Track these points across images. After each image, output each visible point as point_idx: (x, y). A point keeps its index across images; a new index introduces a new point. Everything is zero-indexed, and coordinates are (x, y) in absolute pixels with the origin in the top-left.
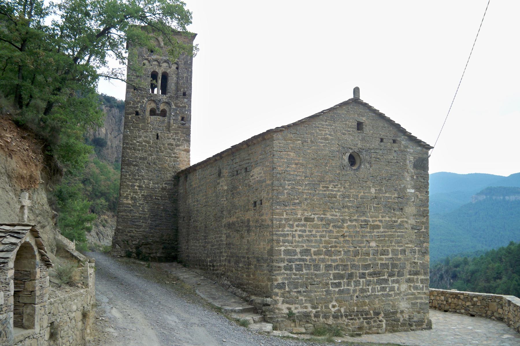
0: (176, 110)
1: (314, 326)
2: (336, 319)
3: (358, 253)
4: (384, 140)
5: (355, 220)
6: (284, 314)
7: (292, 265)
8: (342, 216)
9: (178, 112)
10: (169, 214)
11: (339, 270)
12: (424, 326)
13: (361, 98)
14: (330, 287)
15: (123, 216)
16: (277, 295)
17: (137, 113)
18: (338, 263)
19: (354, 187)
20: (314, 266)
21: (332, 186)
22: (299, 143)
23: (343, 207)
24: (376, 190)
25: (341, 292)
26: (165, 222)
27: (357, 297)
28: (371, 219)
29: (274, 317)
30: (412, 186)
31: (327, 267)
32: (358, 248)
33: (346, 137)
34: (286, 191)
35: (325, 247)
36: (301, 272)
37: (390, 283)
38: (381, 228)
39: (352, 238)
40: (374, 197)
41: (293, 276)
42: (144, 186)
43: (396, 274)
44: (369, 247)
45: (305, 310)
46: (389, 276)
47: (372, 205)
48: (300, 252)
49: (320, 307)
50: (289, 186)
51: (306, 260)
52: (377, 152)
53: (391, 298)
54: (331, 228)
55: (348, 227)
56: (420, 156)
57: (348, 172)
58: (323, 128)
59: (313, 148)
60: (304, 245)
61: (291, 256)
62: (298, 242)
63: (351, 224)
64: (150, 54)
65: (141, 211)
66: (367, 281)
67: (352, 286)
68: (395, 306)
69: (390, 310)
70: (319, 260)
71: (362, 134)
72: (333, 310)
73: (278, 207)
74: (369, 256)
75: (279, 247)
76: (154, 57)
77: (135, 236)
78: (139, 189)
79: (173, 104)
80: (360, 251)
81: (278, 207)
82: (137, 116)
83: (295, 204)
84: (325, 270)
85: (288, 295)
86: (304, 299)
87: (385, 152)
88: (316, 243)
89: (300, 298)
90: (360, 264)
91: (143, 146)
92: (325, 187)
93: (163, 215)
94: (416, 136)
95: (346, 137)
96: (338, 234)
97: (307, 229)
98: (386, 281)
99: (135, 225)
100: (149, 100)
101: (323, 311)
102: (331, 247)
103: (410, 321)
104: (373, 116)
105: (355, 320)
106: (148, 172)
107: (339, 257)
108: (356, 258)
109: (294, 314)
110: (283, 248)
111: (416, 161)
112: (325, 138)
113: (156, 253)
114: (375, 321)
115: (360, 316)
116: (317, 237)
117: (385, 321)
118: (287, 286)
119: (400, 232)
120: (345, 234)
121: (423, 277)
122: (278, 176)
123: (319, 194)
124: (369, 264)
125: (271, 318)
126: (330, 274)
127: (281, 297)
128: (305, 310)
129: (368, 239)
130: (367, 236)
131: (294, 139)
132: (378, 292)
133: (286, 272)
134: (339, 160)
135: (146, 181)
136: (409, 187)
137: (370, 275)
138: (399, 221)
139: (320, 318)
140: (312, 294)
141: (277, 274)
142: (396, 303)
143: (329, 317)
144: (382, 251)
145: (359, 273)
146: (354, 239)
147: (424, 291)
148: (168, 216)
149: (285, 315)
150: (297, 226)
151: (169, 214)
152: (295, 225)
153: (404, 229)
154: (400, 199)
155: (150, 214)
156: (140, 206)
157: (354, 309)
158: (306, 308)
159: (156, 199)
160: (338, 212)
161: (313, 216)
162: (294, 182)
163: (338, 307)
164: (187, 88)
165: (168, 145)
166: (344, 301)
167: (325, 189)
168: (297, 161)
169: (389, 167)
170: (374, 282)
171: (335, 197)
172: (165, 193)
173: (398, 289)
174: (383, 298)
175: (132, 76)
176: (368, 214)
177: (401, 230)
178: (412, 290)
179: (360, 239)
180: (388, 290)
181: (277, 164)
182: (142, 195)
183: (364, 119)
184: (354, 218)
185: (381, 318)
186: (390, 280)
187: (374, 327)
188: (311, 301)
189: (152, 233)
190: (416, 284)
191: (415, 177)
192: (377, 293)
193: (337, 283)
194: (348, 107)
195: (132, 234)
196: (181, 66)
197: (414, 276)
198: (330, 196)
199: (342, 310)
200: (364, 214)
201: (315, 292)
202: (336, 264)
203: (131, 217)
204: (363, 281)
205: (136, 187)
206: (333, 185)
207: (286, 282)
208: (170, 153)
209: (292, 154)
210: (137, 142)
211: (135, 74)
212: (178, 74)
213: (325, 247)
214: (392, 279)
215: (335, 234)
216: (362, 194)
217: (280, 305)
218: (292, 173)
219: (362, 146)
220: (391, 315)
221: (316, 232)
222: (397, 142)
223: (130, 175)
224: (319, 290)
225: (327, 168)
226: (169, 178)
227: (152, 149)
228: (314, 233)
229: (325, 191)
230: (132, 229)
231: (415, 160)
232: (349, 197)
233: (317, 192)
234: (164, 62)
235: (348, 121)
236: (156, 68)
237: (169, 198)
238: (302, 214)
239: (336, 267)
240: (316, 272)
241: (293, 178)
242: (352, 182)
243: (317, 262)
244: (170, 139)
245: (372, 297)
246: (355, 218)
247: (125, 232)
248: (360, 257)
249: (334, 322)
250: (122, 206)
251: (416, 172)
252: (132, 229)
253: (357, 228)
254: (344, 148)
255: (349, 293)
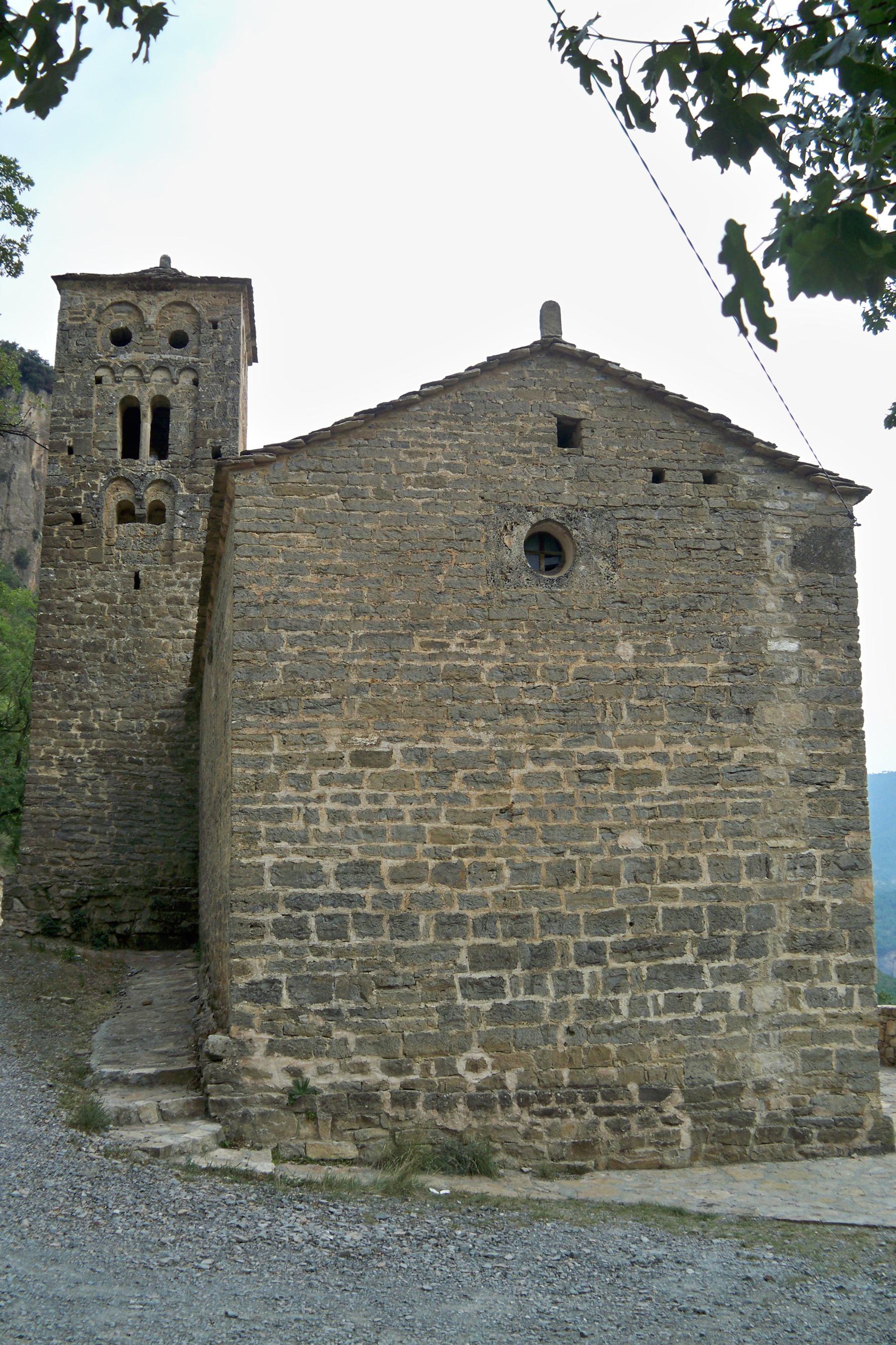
0: (193, 501)
1: (393, 1137)
2: (481, 1113)
3: (569, 874)
4: (668, 475)
5: (556, 755)
6: (277, 1090)
7: (305, 919)
8: (502, 742)
9: (197, 507)
10: (170, 806)
11: (494, 936)
12: (862, 1141)
13: (565, 337)
14: (459, 996)
15: (35, 815)
16: (246, 1021)
17: (78, 519)
18: (491, 908)
19: (547, 641)
20: (392, 919)
21: (460, 641)
22: (330, 502)
23: (506, 713)
24: (638, 648)
25: (501, 1014)
26: (160, 829)
27: (570, 1031)
28: (619, 753)
29: (232, 1101)
30: (790, 631)
31: (443, 924)
32: (568, 855)
33: (515, 471)
34: (280, 665)
35: (436, 854)
36: (339, 944)
37: (709, 982)
38: (665, 782)
39: (545, 819)
40: (634, 673)
41: (310, 958)
42: (97, 726)
43: (733, 948)
44: (616, 850)
45: (359, 1078)
46: (703, 955)
47: (622, 700)
48: (336, 874)
49: (417, 1067)
50: (292, 645)
51: (361, 901)
52: (639, 515)
53: (714, 1036)
54: (457, 786)
55: (526, 780)
56: (819, 521)
57: (524, 591)
58: (421, 445)
59: (387, 513)
60: (354, 847)
61: (302, 886)
62: (330, 837)
63: (537, 769)
64: (116, 351)
65: (88, 799)
66: (610, 974)
67: (546, 993)
68: (733, 1067)
69: (712, 1082)
70: (412, 900)
71: (578, 458)
72: (472, 1078)
73: (249, 719)
74: (618, 885)
75: (254, 854)
76: (127, 357)
77: (71, 873)
78: (82, 737)
79: (182, 485)
80: (578, 866)
81: (249, 719)
82: (76, 527)
83: (316, 706)
84: (437, 933)
85: (291, 1024)
86: (352, 1038)
87: (674, 514)
88: (398, 839)
89: (337, 1034)
90: (581, 912)
91: (94, 609)
92: (433, 645)
93: (155, 808)
94: (794, 453)
95: (515, 471)
96: (489, 807)
97: (364, 792)
98: (691, 973)
99: (73, 841)
100: (112, 481)
101: (432, 1083)
102: (460, 853)
103: (796, 1121)
104: (620, 398)
105: (563, 1115)
106: (110, 683)
107: (495, 888)
108: (561, 892)
109: (315, 1091)
110: (268, 860)
111: (803, 541)
112: (431, 479)
113: (132, 921)
114: (645, 1122)
115: (581, 1102)
116: (401, 818)
117: (688, 1121)
118: (284, 992)
119: (741, 794)
120: (517, 806)
121: (847, 958)
122: (253, 612)
123: (408, 668)
124: (620, 914)
125: (222, 1104)
126: (458, 949)
127: (263, 1031)
128: (359, 1078)
129: (611, 822)
130: (604, 810)
131: (312, 489)
132: (658, 1013)
133: (281, 943)
134: (488, 549)
135: (102, 711)
136: (776, 632)
137: (622, 950)
138: (738, 755)
139: (414, 1106)
140: (387, 1022)
141: (249, 951)
142: (738, 1055)
143: (453, 1103)
144: (672, 863)
145: (577, 945)
146: (552, 823)
147: (857, 1008)
148: (170, 810)
149: (275, 1095)
150: (324, 782)
151: (170, 806)
152: (315, 778)
153: (758, 783)
154: (738, 676)
155: (115, 807)
156: (85, 785)
157: (560, 1078)
158: (362, 1072)
159: (131, 761)
160: (484, 729)
161: (384, 746)
162: (308, 633)
163: (493, 1067)
164: (225, 435)
165: (169, 602)
166: (518, 1048)
167: (432, 651)
168: (323, 563)
169: (688, 566)
170: (638, 978)
171: (475, 679)
172: (159, 742)
173: (742, 1003)
174: (679, 1036)
175: (63, 415)
176: (609, 734)
177: (749, 789)
178: (804, 1005)
179: (575, 821)
180: (698, 1005)
181: (249, 574)
182: (91, 753)
183: (584, 406)
184: (551, 749)
185: (670, 1110)
186: (706, 970)
187: (640, 1142)
188: (382, 1046)
189: (120, 863)
190: (820, 985)
191: (799, 598)
192: (652, 1019)
193: (486, 980)
194: (521, 372)
195: (63, 867)
196: (207, 374)
197: (811, 952)
198: (454, 673)
199: (511, 1080)
200: (591, 732)
201: (398, 1012)
202: (482, 912)
203: (58, 818)
204: (593, 974)
205: (73, 731)
206: (467, 637)
207: (283, 977)
208: (173, 627)
209: (303, 538)
210: (78, 600)
211: (71, 410)
212: (196, 399)
213: (436, 854)
214: (716, 964)
215: (474, 806)
216: (582, 663)
217: (258, 1059)
218: (303, 602)
219: (578, 497)
220: (715, 1100)
221: (399, 803)
222: (719, 477)
223: (55, 697)
224: (413, 1006)
225: (440, 579)
226: (172, 700)
227: (120, 617)
228: (390, 803)
229: (432, 657)
230: (64, 854)
231: (798, 537)
232: (527, 675)
233: (402, 663)
234: (156, 369)
235: (519, 418)
236: (133, 389)
237: (172, 756)
238: (344, 742)
239: (484, 925)
240: (399, 943)
241: (307, 620)
242: (538, 624)
243: (403, 907)
244: (173, 584)
245: (635, 1033)
246: (557, 747)
247: (42, 861)
248: (577, 886)
249: (475, 1124)
250: (32, 786)
251: (803, 577)
252: (64, 854)
253: (565, 785)
254: (504, 507)
255: (538, 1019)
